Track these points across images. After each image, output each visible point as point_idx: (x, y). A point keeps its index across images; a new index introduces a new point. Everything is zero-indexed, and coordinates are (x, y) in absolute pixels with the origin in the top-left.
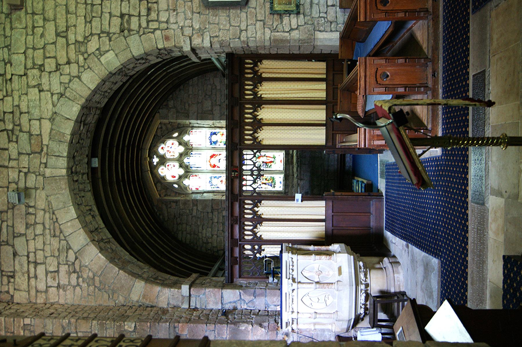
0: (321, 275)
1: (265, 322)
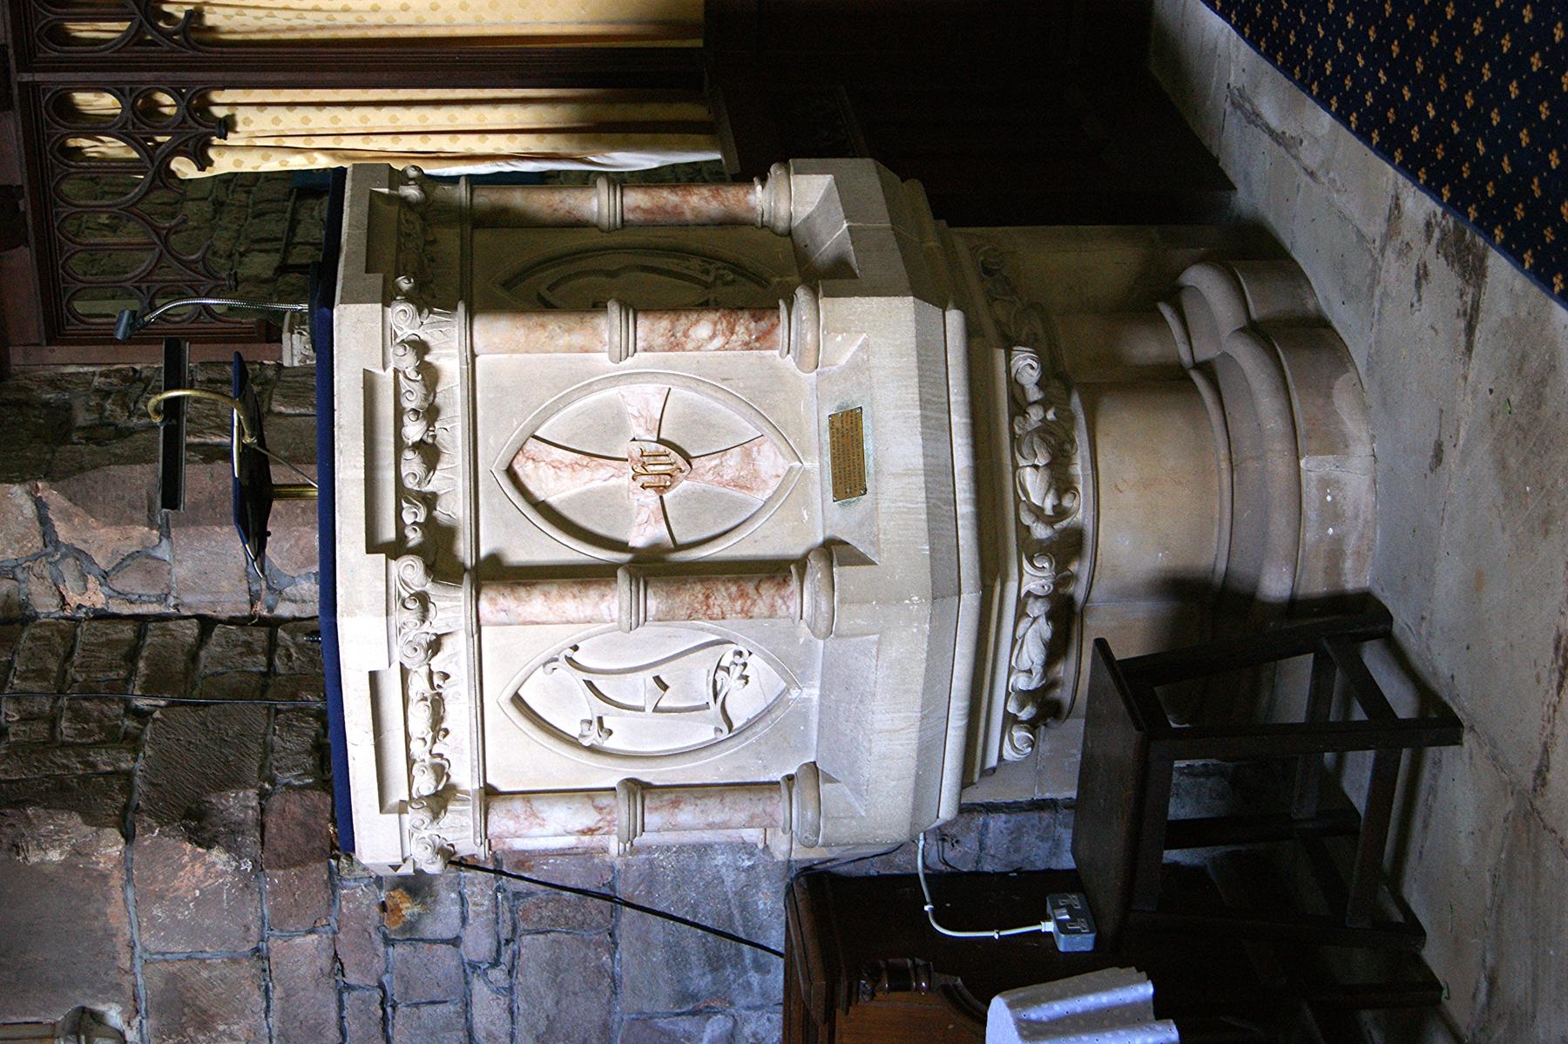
0: (683, 485)
1: (234, 781)
